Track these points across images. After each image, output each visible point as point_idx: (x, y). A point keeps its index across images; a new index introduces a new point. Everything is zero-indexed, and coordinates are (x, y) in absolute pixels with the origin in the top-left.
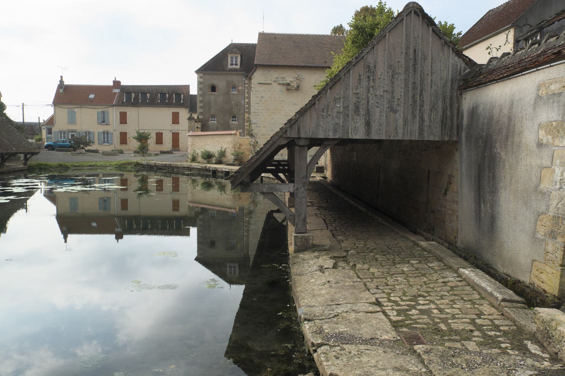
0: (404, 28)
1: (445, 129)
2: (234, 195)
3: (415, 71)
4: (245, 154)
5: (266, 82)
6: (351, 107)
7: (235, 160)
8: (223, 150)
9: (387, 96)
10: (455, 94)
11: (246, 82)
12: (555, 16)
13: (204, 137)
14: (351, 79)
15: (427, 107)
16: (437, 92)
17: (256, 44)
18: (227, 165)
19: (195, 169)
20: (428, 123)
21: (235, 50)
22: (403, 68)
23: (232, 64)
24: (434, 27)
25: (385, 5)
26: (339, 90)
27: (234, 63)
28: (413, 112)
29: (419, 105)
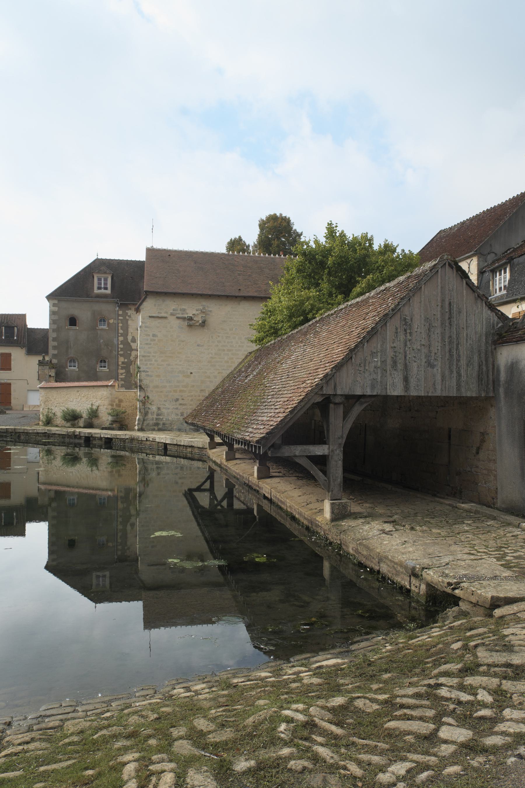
0: (439, 281)
1: (482, 384)
2: (111, 472)
3: (450, 325)
4: (127, 413)
5: (160, 315)
6: (389, 361)
7: (114, 422)
8: (95, 407)
9: (424, 350)
10: (490, 348)
11: (120, 312)
12: (522, 243)
13: (65, 390)
14: (388, 333)
15: (463, 362)
16: (472, 347)
17: (144, 261)
18: (103, 429)
19: (57, 436)
20: (465, 378)
21: (103, 268)
22: (439, 321)
23: (99, 288)
24: (467, 280)
25: (336, 226)
26: (376, 344)
27: (103, 286)
28: (450, 367)
29: (455, 360)
